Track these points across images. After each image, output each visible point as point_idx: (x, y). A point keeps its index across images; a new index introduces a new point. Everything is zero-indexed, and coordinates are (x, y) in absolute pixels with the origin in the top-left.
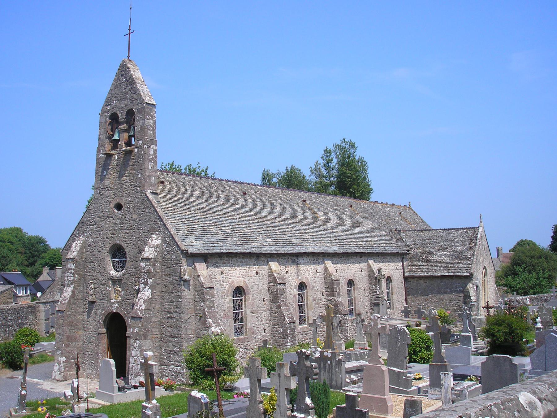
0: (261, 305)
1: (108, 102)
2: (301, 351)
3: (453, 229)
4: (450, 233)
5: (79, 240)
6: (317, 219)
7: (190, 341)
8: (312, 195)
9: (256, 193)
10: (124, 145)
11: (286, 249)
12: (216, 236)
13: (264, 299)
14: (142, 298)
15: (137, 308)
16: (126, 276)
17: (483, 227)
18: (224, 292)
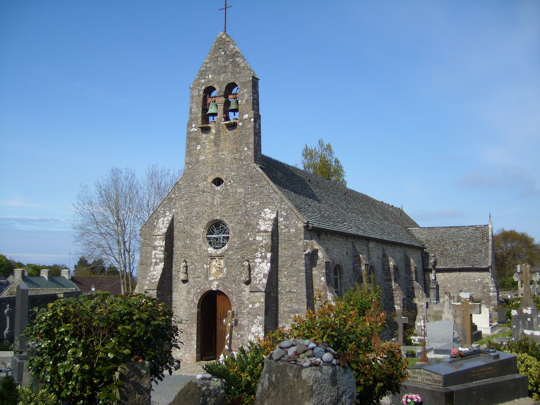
1: (202, 74)
4: (460, 230)
5: (166, 216)
14: (261, 272)
15: (256, 283)
16: (230, 253)
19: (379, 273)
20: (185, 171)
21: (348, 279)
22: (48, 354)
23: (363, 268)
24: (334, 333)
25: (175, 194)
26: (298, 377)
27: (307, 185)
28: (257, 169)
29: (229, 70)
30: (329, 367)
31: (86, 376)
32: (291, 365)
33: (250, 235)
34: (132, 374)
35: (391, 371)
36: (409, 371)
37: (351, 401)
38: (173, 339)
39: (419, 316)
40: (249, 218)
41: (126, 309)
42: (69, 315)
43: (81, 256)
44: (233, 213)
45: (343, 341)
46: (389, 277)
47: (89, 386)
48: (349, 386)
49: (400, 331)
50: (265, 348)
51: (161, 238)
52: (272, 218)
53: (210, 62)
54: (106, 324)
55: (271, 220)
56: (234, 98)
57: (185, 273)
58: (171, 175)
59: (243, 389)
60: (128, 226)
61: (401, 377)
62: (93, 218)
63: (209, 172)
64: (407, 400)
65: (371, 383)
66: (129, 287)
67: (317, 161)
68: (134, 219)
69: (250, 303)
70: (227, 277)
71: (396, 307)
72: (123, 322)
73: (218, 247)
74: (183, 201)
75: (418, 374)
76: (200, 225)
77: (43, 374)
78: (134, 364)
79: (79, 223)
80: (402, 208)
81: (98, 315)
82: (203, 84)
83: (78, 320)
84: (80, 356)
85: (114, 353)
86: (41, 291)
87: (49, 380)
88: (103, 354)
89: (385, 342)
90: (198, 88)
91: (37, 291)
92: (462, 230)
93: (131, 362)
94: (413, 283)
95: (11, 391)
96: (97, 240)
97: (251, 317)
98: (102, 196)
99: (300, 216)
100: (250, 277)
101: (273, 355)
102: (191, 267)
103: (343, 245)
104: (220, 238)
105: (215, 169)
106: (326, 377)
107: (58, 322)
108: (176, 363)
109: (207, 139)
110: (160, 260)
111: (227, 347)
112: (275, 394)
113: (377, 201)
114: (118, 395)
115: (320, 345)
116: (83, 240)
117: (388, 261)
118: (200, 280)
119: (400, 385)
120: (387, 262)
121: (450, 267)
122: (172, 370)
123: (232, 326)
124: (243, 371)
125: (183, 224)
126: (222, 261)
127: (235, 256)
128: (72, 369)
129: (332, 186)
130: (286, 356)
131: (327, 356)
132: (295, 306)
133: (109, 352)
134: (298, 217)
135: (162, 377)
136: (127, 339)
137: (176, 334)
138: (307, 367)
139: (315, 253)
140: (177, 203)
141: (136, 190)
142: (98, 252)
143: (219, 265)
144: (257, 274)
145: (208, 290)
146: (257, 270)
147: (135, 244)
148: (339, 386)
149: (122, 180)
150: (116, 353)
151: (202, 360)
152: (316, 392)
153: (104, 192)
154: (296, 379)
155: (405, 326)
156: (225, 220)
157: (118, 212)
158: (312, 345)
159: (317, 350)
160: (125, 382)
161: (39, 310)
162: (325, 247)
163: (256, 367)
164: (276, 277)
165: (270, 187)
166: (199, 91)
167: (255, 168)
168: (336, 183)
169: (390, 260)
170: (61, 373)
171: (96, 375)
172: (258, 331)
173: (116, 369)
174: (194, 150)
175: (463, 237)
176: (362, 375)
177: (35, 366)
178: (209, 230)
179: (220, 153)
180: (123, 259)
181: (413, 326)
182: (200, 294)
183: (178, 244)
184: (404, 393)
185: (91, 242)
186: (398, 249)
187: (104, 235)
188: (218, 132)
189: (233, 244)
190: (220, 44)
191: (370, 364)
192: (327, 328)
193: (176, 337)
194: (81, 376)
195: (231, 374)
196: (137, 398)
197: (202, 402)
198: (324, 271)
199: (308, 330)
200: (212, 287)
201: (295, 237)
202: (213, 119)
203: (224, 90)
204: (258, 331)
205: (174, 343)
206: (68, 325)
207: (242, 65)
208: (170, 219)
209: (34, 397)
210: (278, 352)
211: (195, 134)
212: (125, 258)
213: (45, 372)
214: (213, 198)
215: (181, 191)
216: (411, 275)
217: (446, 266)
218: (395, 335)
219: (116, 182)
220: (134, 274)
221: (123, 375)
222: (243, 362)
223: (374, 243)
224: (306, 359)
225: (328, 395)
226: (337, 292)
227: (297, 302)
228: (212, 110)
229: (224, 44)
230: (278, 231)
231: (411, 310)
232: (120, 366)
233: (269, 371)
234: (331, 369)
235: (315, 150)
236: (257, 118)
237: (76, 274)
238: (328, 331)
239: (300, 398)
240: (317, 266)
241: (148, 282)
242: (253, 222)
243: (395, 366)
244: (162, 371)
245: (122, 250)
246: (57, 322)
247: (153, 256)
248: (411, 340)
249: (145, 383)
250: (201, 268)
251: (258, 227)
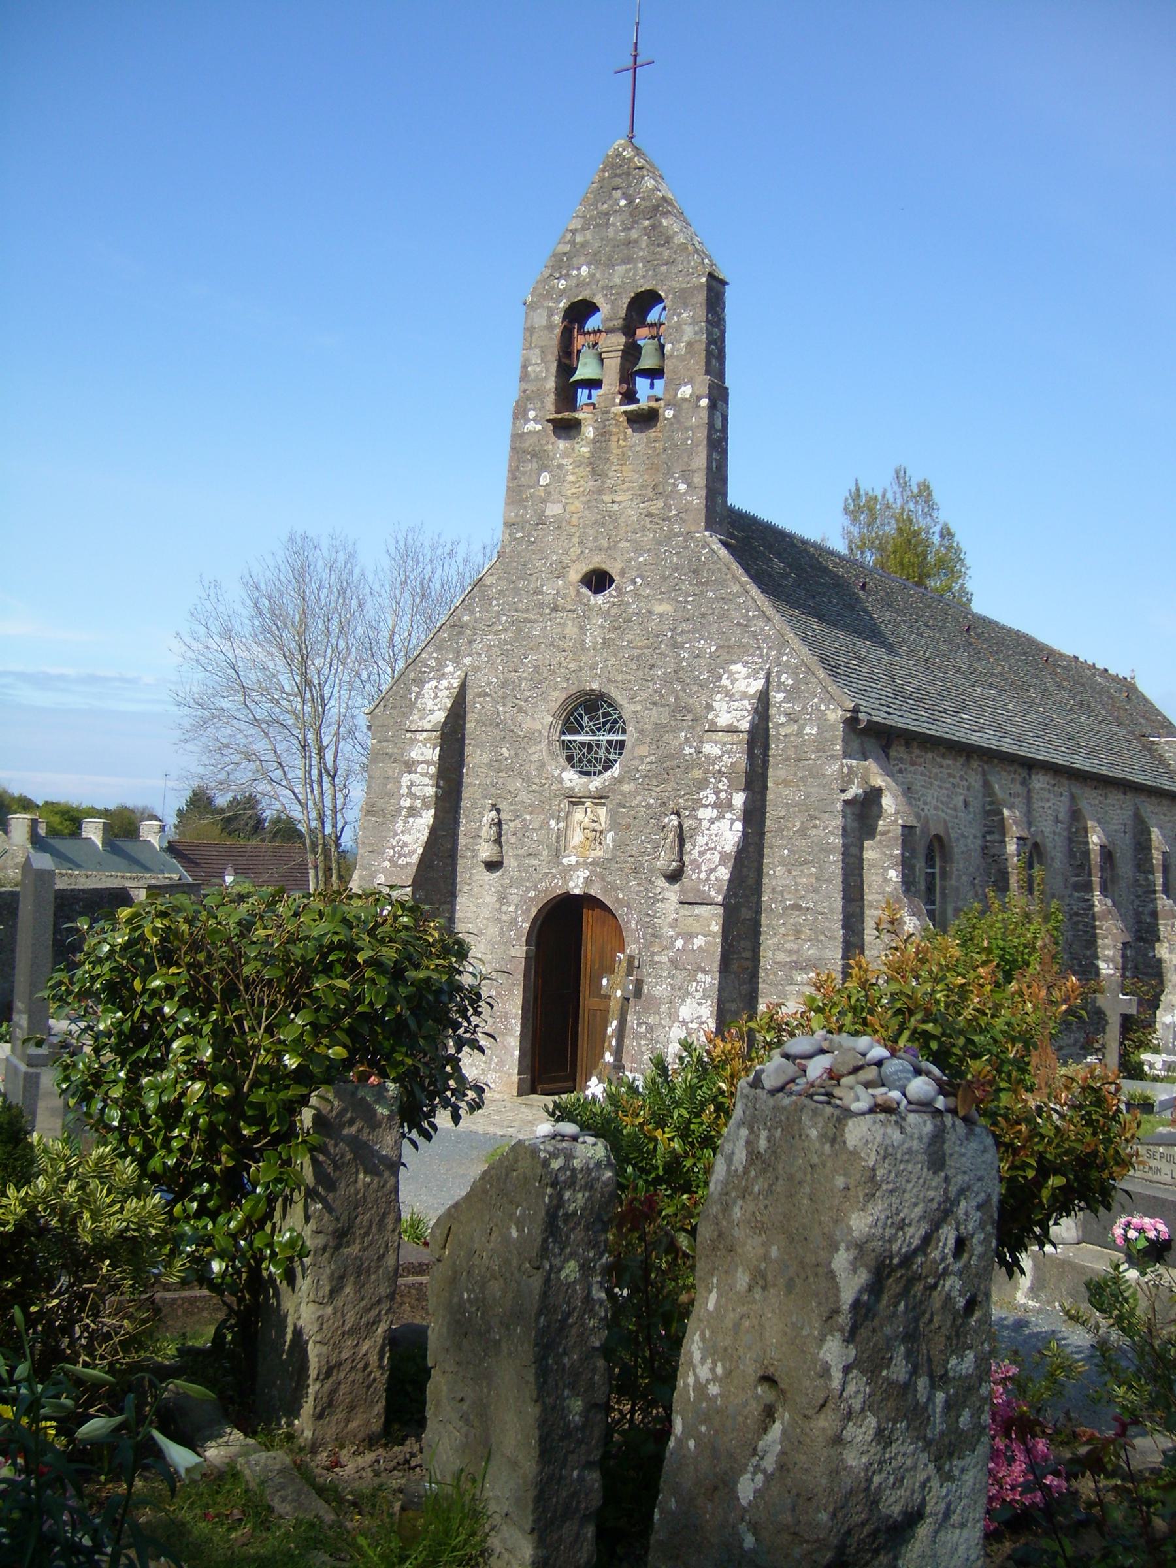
1: (561, 263)
14: (714, 848)
16: (626, 787)
19: (1057, 864)
20: (503, 547)
21: (964, 878)
22: (115, 1050)
23: (1012, 847)
24: (929, 1027)
25: (472, 613)
26: (833, 1141)
27: (858, 600)
28: (714, 547)
29: (641, 254)
30: (926, 1117)
31: (221, 1116)
32: (814, 1105)
33: (686, 739)
34: (349, 1115)
35: (1088, 1145)
36: (1142, 1150)
37: (981, 1218)
38: (465, 1024)
39: (1170, 997)
40: (683, 690)
41: (336, 933)
42: (176, 943)
43: (196, 783)
44: (640, 673)
45: (956, 1051)
46: (1086, 878)
47: (228, 1143)
48: (979, 1173)
49: (1112, 1035)
50: (725, 1062)
51: (430, 739)
52: (751, 691)
53: (583, 229)
54: (280, 974)
55: (750, 698)
56: (653, 338)
57: (495, 841)
58: (459, 558)
59: (658, 1175)
60: (332, 702)
61: (1117, 1164)
62: (234, 675)
63: (575, 551)
64: (1126, 1232)
65: (1031, 1174)
66: (331, 876)
67: (887, 528)
68: (351, 683)
69: (679, 934)
70: (613, 858)
71: (1102, 965)
72: (328, 969)
73: (592, 769)
74: (495, 634)
75: (1164, 1160)
76: (542, 706)
77: (100, 1105)
78: (357, 1088)
79: (195, 690)
80: (1133, 678)
81: (258, 946)
82: (562, 293)
83: (201, 957)
84: (205, 1059)
85: (300, 1055)
86: (83, 880)
87: (115, 1124)
88: (269, 1057)
89: (1065, 1064)
90: (546, 304)
91: (73, 880)
93: (347, 1081)
94: (1156, 899)
95: (14, 1148)
96: (244, 740)
97: (680, 976)
98: (261, 614)
99: (832, 688)
100: (681, 860)
101: (763, 1076)
102: (512, 824)
103: (954, 777)
104: (598, 745)
105: (590, 545)
106: (915, 1144)
107: (146, 961)
108: (471, 1094)
109: (568, 456)
110: (424, 803)
111: (608, 1057)
112: (766, 1186)
113: (1061, 655)
114: (308, 1174)
115: (901, 1054)
116: (204, 739)
117: (1086, 832)
118: (536, 862)
119: (1114, 1187)
120: (1083, 833)
122: (461, 1112)
123: (627, 999)
124: (661, 1124)
125: (493, 699)
126: (602, 812)
127: (639, 798)
128: (183, 1094)
129: (929, 607)
130: (802, 1081)
131: (920, 1086)
132: (809, 949)
133: (287, 1052)
134: (828, 692)
135: (432, 1132)
136: (338, 1016)
137: (475, 1010)
138: (863, 1114)
139: (872, 797)
140: (479, 639)
141: (358, 598)
142: (244, 774)
143: (594, 821)
144: (701, 853)
145: (558, 892)
146: (701, 840)
147: (351, 755)
148: (950, 1172)
149: (319, 569)
150: (307, 1055)
151: (533, 1091)
152: (884, 1187)
153: (266, 603)
154: (827, 1147)
155: (1127, 1023)
156: (614, 693)
157: (304, 662)
158: (878, 1052)
159: (893, 1066)
160: (329, 1136)
161: (91, 927)
162: (903, 783)
163: (698, 1115)
164: (755, 864)
165: (750, 603)
167: (706, 545)
168: (941, 596)
169: (1093, 827)
170: (151, 1105)
171: (250, 1113)
172: (698, 1017)
173: (304, 1101)
174: (531, 487)
176: (1007, 1151)
177: (78, 1082)
178: (567, 721)
179: (607, 498)
180: (317, 797)
181: (1150, 1024)
182: (536, 906)
183: (476, 757)
184: (1123, 1210)
185: (227, 746)
186: (1115, 798)
187: (264, 726)
188: (602, 435)
189: (635, 763)
190: (616, 176)
191: (1029, 1120)
192: (912, 1013)
193: (475, 1020)
194: (207, 1114)
195: (625, 1132)
196: (360, 1184)
197: (550, 1201)
198: (898, 852)
199: (855, 1015)
200: (571, 884)
201: (818, 750)
202: (590, 397)
203: (623, 312)
205: (468, 1035)
206: (173, 970)
207: (680, 239)
208: (456, 683)
209: (77, 1167)
210: (778, 1069)
211: (534, 439)
212: (322, 794)
213: (104, 1100)
214: (582, 628)
215: (490, 604)
216: (1150, 877)
218: (1096, 1046)
219: (301, 574)
220: (346, 841)
221: (324, 1116)
222: (661, 1099)
223: (1047, 778)
224: (860, 1089)
225: (917, 1197)
226: (931, 914)
227: (817, 936)
228: (585, 370)
229: (628, 174)
230: (767, 729)
231: (1145, 978)
232: (316, 1093)
233: (750, 1123)
234: (929, 1123)
235: (884, 496)
236: (719, 396)
237: (182, 834)
238: (912, 1019)
239: (836, 1202)
240: (878, 837)
241: (387, 864)
242: (697, 703)
243: (1102, 1130)
244: (432, 1112)
245: (315, 772)
246: (142, 961)
247: (404, 791)
248: (1141, 1064)
249: (385, 1142)
250: (541, 828)
251: (710, 717)
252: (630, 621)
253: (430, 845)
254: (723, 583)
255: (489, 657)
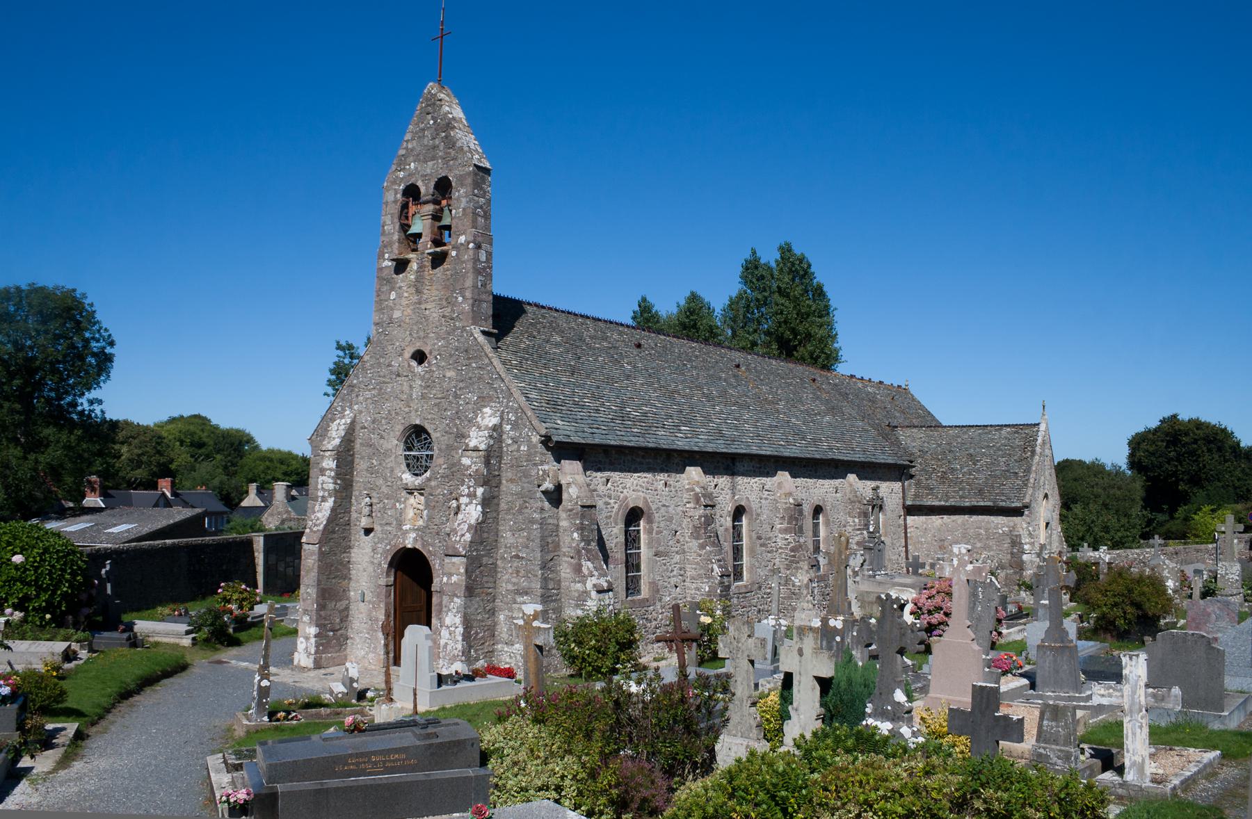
0: (671, 543)
2: (888, 596)
3: (991, 426)
4: (986, 433)
6: (759, 398)
7: (552, 601)
8: (749, 357)
9: (656, 345)
10: (430, 243)
11: (715, 445)
12: (597, 415)
13: (676, 532)
16: (433, 483)
17: (1047, 424)
18: (611, 516)
29: (440, 154)
90: (394, 187)
92: (989, 433)
102: (378, 505)
105: (415, 335)
121: (953, 504)
127: (440, 490)
144: (459, 525)
166: (396, 192)
174: (386, 301)
175: (988, 446)
178: (406, 442)
179: (423, 307)
183: (361, 465)
200: (407, 542)
201: (527, 461)
204: (455, 624)
208: (349, 421)
217: (947, 501)
229: (434, 104)
252: (434, 382)
253: (330, 520)
254: (480, 358)
255: (367, 405)
